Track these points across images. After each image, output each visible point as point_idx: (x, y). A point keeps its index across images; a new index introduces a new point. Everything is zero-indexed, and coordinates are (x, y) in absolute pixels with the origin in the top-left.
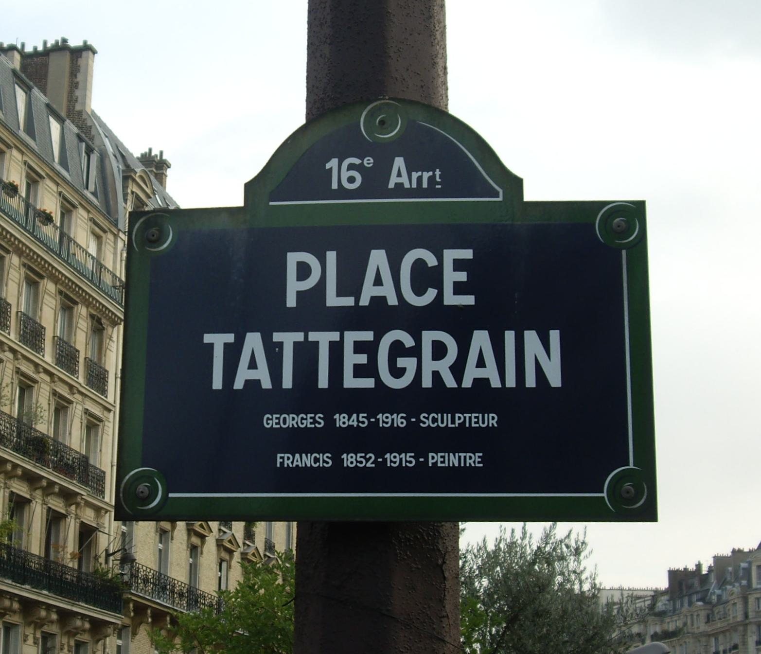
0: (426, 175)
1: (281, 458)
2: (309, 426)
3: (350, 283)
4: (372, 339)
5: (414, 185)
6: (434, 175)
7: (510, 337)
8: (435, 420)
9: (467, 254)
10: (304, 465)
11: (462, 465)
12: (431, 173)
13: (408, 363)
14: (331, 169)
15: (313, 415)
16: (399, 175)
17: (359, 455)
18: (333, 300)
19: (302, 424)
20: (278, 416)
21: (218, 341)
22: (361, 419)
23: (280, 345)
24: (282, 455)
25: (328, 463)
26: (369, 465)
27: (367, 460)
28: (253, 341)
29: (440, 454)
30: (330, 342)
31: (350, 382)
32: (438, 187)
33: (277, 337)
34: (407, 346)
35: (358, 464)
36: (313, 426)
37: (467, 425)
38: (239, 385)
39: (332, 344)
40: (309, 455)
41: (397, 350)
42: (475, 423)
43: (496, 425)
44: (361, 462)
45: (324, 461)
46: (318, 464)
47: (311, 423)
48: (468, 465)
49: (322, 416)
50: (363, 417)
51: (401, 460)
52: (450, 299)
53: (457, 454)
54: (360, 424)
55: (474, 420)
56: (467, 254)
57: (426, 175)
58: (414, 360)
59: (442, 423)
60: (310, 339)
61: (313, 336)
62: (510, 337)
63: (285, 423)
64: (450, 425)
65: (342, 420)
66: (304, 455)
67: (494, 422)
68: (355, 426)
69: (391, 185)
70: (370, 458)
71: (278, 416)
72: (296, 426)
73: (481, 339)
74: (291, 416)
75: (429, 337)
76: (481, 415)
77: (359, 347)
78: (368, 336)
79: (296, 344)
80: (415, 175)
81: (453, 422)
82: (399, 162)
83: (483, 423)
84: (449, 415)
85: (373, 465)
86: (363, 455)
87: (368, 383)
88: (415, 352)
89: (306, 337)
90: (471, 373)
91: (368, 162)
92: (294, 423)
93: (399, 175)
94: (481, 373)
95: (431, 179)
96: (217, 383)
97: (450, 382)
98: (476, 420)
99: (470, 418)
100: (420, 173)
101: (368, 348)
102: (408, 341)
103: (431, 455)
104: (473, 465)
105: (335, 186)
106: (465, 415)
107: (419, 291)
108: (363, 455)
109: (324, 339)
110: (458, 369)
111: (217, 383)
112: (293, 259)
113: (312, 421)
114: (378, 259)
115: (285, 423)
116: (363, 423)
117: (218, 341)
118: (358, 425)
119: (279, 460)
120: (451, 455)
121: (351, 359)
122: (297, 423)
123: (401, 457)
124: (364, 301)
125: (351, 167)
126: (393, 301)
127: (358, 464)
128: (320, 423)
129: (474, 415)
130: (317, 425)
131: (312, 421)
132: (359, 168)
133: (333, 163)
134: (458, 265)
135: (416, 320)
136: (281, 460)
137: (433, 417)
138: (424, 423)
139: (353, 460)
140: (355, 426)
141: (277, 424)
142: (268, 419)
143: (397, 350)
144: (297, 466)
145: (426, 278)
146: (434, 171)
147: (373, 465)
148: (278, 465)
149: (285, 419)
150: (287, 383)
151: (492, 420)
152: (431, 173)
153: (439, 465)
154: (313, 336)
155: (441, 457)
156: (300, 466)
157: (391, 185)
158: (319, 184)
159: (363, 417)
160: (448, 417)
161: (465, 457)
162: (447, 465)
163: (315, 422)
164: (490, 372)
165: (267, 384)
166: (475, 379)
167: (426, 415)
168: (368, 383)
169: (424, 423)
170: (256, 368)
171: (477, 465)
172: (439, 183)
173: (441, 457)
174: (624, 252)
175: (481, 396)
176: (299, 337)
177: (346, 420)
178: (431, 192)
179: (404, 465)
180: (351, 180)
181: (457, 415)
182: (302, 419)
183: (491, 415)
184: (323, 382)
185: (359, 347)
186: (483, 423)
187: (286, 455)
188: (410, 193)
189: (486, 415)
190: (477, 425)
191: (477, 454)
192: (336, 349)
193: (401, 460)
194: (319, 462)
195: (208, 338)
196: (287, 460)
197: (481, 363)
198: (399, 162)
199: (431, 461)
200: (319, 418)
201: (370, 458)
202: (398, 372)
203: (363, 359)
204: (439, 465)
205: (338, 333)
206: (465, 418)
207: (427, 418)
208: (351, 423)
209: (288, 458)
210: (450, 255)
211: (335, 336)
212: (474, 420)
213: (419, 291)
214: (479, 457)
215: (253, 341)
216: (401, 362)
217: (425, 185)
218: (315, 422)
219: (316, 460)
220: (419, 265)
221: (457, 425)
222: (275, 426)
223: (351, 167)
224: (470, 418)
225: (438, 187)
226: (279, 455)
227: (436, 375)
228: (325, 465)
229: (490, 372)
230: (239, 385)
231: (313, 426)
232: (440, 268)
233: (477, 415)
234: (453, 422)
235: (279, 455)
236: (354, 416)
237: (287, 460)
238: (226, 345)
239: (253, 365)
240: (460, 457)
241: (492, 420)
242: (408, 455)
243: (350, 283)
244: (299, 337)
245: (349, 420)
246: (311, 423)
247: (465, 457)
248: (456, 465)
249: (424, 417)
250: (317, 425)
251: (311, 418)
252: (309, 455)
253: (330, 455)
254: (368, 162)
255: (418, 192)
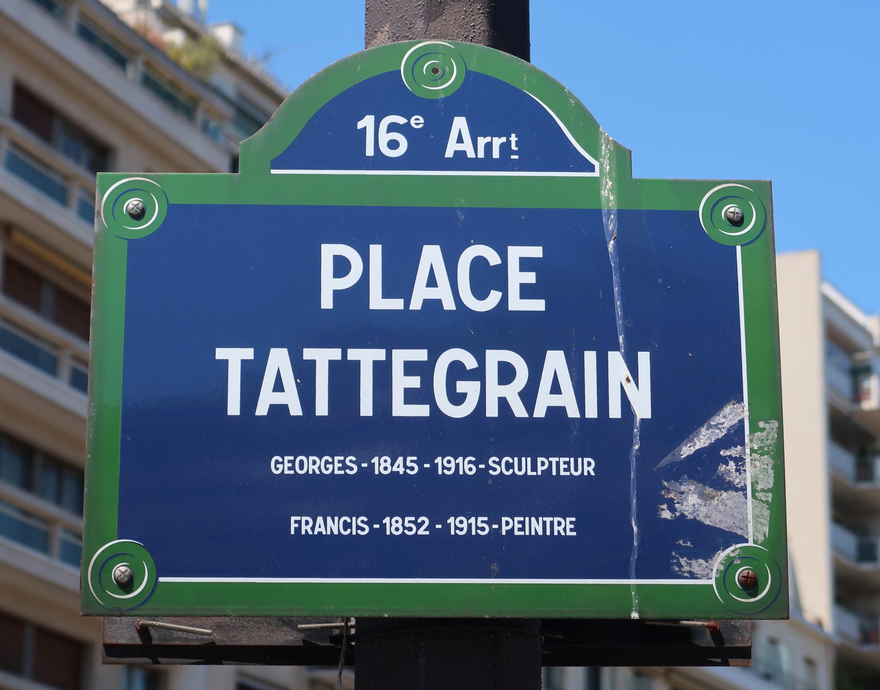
0: (497, 142)
1: (296, 522)
2: (337, 472)
3: (399, 281)
4: (426, 359)
5: (481, 154)
6: (509, 142)
7: (590, 358)
8: (509, 466)
9: (536, 252)
10: (329, 533)
11: (548, 533)
12: (504, 139)
13: (469, 388)
14: (365, 128)
15: (342, 458)
16: (460, 140)
17: (407, 519)
18: (377, 301)
19: (327, 469)
20: (292, 458)
21: (234, 357)
22: (409, 464)
23: (313, 363)
24: (298, 518)
25: (363, 529)
26: (421, 532)
27: (419, 526)
28: (279, 360)
29: (517, 519)
30: (374, 362)
31: (400, 409)
32: (513, 157)
33: (309, 354)
34: (468, 368)
35: (406, 531)
36: (342, 472)
37: (554, 473)
38: (262, 410)
39: (376, 363)
40: (336, 518)
41: (456, 371)
42: (565, 470)
43: (593, 474)
44: (410, 529)
45: (358, 527)
46: (349, 530)
47: (339, 469)
48: (556, 533)
49: (354, 459)
50: (412, 461)
51: (470, 526)
52: (516, 304)
53: (540, 519)
54: (408, 471)
55: (563, 466)
56: (536, 252)
57: (497, 142)
58: (477, 384)
59: (520, 469)
60: (350, 358)
61: (353, 354)
62: (590, 358)
63: (301, 468)
64: (530, 473)
65: (383, 465)
66: (329, 519)
67: (591, 469)
68: (401, 473)
69: (449, 154)
70: (423, 522)
71: (292, 458)
72: (318, 472)
73: (555, 361)
74: (311, 458)
75: (494, 357)
76: (572, 460)
77: (410, 368)
78: (421, 355)
79: (332, 363)
80: (482, 141)
81: (534, 468)
82: (460, 124)
83: (576, 470)
84: (529, 459)
85: (427, 533)
86: (413, 519)
87: (422, 411)
88: (479, 375)
89: (344, 354)
90: (544, 401)
91: (417, 122)
92: (316, 467)
93: (460, 140)
94: (556, 401)
95: (505, 147)
96: (234, 408)
97: (519, 410)
98: (566, 466)
99: (558, 463)
100: (488, 139)
101: (424, 370)
102: (470, 362)
103: (504, 519)
104: (563, 533)
105: (370, 152)
106: (550, 459)
107: (480, 293)
108: (413, 519)
109: (366, 358)
110: (529, 396)
111: (234, 408)
112: (329, 251)
113: (340, 465)
114: (431, 256)
115: (301, 468)
116: (412, 469)
117: (234, 357)
118: (405, 472)
119: (294, 526)
120: (533, 519)
121: (401, 382)
122: (319, 468)
123: (470, 522)
124: (416, 304)
125: (392, 128)
126: (449, 305)
127: (406, 531)
128: (352, 469)
129: (562, 460)
130: (348, 471)
131: (340, 465)
132: (405, 130)
133: (367, 122)
134: (526, 264)
135: (481, 332)
136: (297, 525)
137: (507, 462)
138: (495, 470)
139: (399, 525)
140: (401, 473)
141: (289, 469)
142: (277, 462)
143: (456, 371)
144: (320, 533)
145: (487, 278)
146: (508, 137)
147: (427, 533)
148: (293, 532)
149: (301, 463)
150: (322, 408)
151: (587, 466)
152: (504, 139)
153: (517, 533)
154: (353, 354)
155: (519, 522)
156: (324, 533)
157: (449, 154)
158: (350, 150)
159: (412, 461)
160: (526, 462)
161: (552, 523)
162: (527, 533)
163: (344, 467)
164: (567, 400)
165: (296, 410)
166: (564, 408)
167: (497, 459)
168: (422, 411)
169: (495, 470)
170: (283, 391)
171: (569, 533)
172: (515, 153)
173: (519, 522)
174: (739, 248)
175: (555, 433)
176: (336, 354)
177: (388, 465)
178: (504, 163)
179: (474, 533)
180: (393, 145)
181: (540, 460)
182: (327, 462)
183: (586, 460)
184: (366, 409)
185: (410, 368)
186: (576, 470)
187: (304, 519)
188: (476, 164)
189: (580, 460)
190: (568, 474)
191: (568, 519)
192: (383, 371)
193: (470, 526)
194: (351, 528)
195: (221, 353)
196: (303, 524)
197: (556, 389)
198: (460, 124)
199: (504, 529)
200: (351, 461)
201: (423, 522)
202: (457, 399)
203: (415, 382)
204: (517, 533)
205: (384, 351)
206: (550, 463)
207: (499, 463)
208: (395, 469)
209: (307, 523)
210: (515, 253)
211: (380, 354)
212: (563, 466)
213: (480, 293)
214: (571, 523)
215: (279, 360)
216: (462, 386)
217: (496, 154)
218: (344, 467)
219: (347, 526)
220: (479, 263)
221: (539, 473)
222: (287, 472)
223: (392, 128)
224: (558, 463)
225: (513, 157)
226: (293, 519)
227: (503, 403)
228: (359, 532)
229: (567, 400)
230: (262, 410)
231: (342, 472)
232: (503, 268)
233: (567, 459)
234: (534, 468)
235: (293, 519)
236: (400, 460)
237: (303, 524)
238: (244, 363)
239: (279, 387)
240: (544, 523)
241: (587, 466)
242: (480, 519)
243: (399, 281)
244: (336, 354)
245: (392, 465)
246: (339, 469)
247: (552, 523)
248: (540, 533)
249: (494, 462)
250: (348, 471)
251: (339, 462)
252: (336, 518)
253: (365, 519)
254: (417, 122)
255: (487, 163)
